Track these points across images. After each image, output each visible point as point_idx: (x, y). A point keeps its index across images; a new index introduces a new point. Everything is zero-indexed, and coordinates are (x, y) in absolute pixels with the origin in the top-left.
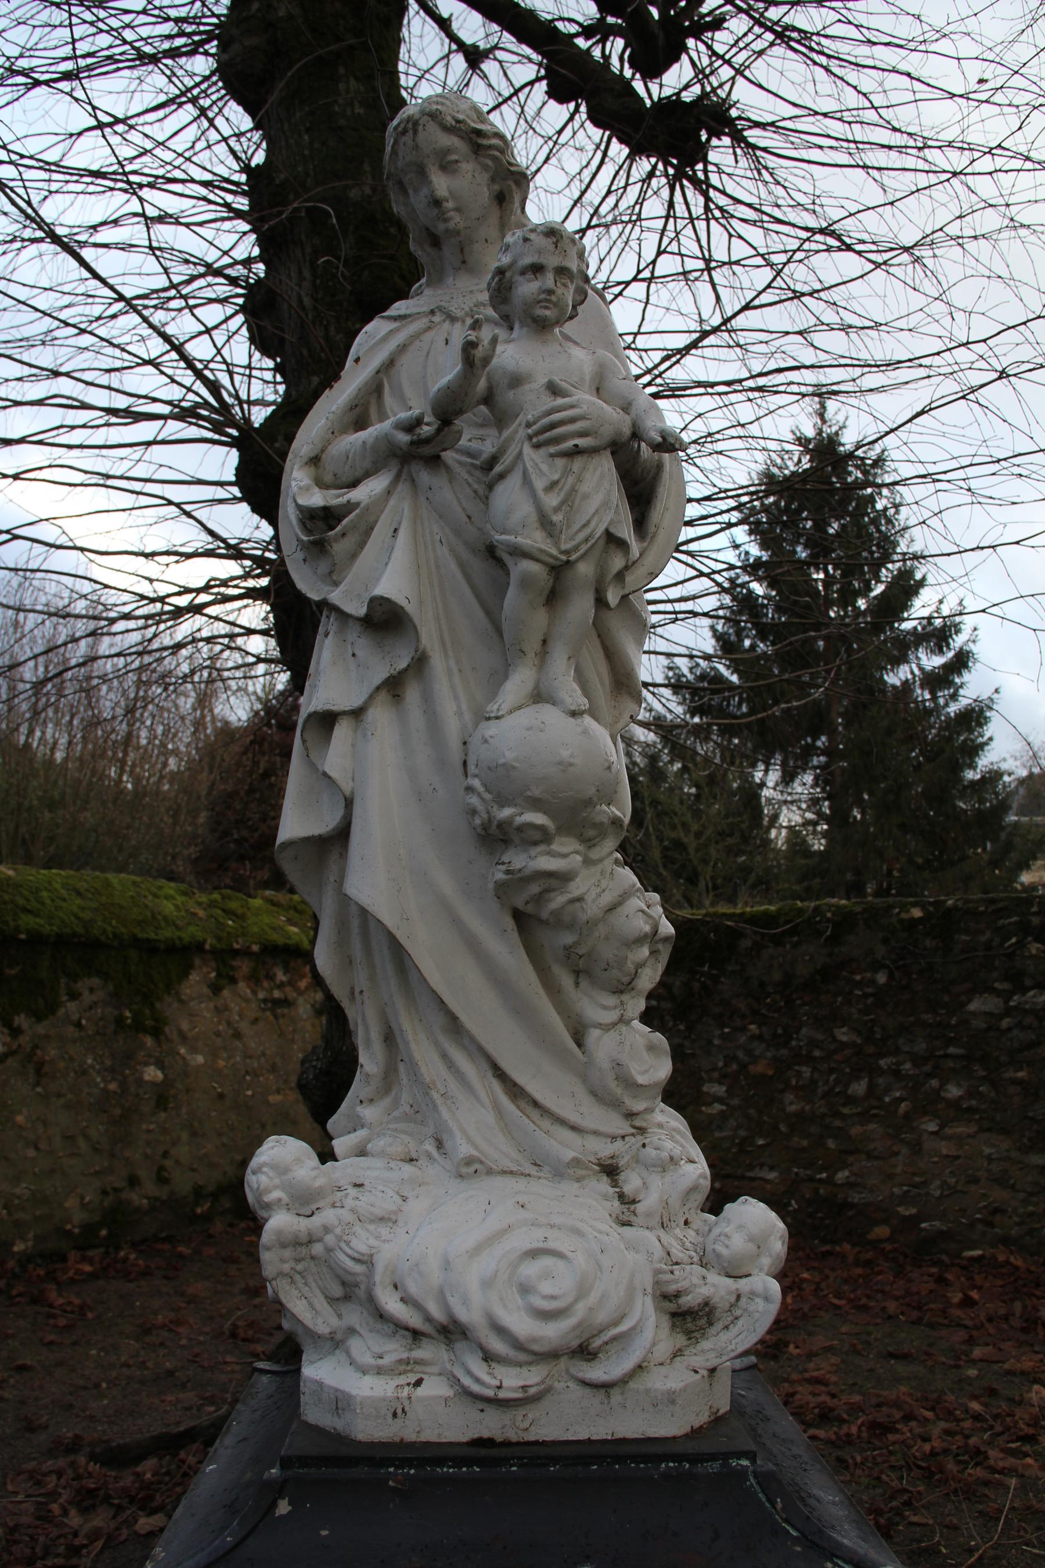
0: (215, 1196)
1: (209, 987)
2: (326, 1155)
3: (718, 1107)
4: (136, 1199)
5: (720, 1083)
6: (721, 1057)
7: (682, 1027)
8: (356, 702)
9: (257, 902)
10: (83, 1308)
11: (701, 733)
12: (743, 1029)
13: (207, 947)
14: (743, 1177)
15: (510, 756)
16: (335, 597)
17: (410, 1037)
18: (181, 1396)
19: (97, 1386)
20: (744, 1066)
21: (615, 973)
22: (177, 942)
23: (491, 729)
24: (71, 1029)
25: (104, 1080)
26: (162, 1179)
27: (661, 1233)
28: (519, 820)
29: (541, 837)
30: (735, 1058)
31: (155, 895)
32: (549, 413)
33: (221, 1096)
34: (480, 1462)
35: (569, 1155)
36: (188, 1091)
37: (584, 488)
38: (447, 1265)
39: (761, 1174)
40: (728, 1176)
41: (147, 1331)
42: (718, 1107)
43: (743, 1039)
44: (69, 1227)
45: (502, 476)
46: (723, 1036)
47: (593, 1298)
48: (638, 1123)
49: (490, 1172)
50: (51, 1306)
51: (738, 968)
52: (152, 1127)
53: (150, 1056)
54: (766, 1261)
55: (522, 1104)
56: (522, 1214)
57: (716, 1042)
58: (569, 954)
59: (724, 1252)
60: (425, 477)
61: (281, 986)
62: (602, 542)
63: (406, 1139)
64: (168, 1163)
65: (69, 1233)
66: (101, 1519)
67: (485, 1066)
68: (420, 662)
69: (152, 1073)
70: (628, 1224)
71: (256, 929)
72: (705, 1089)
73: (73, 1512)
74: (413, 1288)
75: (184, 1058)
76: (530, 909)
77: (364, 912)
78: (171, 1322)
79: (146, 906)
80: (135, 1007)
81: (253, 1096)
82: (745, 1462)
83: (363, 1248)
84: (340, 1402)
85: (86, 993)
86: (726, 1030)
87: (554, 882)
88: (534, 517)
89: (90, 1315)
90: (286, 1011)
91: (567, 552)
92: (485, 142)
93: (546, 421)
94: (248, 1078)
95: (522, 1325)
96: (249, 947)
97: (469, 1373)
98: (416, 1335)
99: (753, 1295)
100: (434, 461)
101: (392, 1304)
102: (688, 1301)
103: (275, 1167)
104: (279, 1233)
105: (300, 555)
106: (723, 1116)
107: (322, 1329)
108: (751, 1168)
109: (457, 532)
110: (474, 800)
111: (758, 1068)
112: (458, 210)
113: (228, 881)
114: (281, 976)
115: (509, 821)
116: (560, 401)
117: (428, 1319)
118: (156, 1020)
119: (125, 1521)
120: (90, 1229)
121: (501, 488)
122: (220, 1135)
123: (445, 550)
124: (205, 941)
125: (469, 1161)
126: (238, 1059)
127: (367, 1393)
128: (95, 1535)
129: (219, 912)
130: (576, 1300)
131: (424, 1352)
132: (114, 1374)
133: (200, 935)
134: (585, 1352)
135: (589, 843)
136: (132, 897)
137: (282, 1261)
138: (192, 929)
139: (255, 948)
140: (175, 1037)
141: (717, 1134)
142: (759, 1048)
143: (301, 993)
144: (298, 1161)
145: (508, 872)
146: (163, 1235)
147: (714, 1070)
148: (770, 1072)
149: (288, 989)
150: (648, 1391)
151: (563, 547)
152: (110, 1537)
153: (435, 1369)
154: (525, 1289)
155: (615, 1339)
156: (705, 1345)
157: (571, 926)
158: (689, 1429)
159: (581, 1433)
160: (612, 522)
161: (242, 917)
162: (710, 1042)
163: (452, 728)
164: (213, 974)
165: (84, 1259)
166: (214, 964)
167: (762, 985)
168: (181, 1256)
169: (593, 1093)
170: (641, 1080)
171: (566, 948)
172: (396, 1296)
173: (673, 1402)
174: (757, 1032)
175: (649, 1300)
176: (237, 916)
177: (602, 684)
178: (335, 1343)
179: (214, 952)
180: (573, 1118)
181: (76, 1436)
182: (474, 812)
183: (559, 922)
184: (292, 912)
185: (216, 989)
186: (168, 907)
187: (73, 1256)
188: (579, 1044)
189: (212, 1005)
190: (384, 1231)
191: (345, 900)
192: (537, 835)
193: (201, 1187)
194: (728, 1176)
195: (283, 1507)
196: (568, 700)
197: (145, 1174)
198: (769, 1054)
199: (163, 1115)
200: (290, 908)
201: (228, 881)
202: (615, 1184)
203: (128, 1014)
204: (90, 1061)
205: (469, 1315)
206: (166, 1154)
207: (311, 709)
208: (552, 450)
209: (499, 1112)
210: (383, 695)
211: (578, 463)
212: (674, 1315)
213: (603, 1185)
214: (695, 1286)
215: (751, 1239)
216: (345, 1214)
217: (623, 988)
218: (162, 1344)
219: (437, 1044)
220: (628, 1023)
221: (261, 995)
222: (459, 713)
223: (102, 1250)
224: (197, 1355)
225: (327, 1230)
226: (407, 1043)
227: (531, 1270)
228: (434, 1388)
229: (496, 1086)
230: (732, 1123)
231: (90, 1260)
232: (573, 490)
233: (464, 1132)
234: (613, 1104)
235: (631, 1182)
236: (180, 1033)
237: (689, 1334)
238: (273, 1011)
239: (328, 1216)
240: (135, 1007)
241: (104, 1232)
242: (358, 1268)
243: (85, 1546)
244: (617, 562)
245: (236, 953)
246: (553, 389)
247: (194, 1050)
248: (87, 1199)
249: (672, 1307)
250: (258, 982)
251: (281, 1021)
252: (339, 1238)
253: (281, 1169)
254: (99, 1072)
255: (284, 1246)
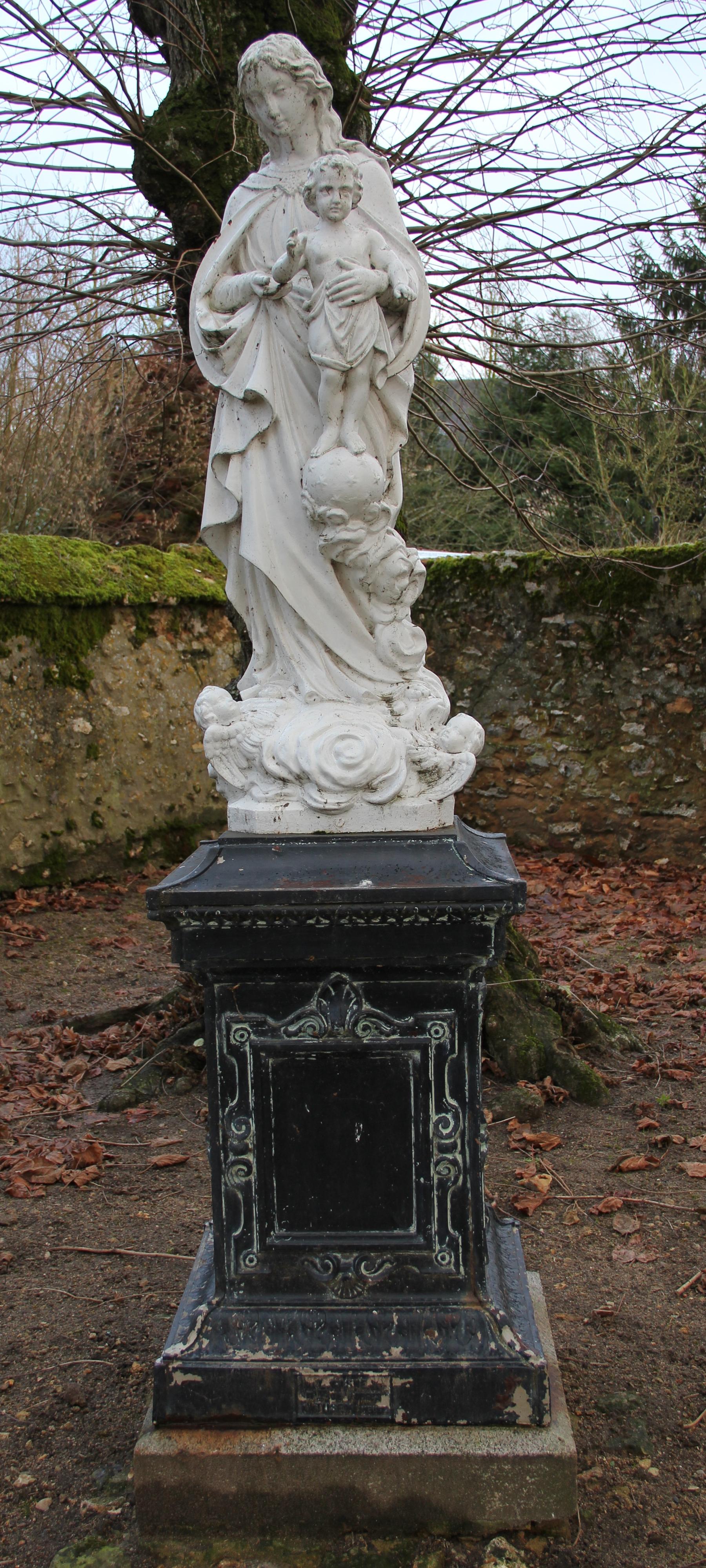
0: (147, 840)
1: (129, 640)
2: (237, 698)
3: (636, 746)
4: (74, 842)
5: (638, 723)
6: (639, 696)
7: (601, 667)
8: (241, 448)
9: (171, 556)
10: (37, 933)
11: (670, 331)
12: (661, 668)
13: (126, 602)
14: (661, 815)
15: (322, 479)
16: (225, 386)
17: (279, 631)
18: (131, 990)
19: (60, 984)
20: (662, 705)
21: (388, 593)
22: (97, 598)
23: (313, 464)
24: (4, 685)
25: (38, 733)
26: (97, 825)
27: (414, 732)
28: (329, 513)
29: (343, 521)
30: (653, 697)
31: (72, 553)
32: (338, 282)
33: (147, 745)
34: (317, 840)
35: (364, 690)
36: (116, 741)
37: (359, 324)
38: (299, 744)
39: (679, 812)
40: (647, 814)
41: (98, 947)
42: (636, 746)
43: (661, 678)
44: (15, 868)
45: (314, 318)
46: (641, 676)
47: (373, 759)
48: (407, 677)
49: (322, 700)
50: (8, 930)
51: (656, 606)
52: (84, 775)
53: (78, 708)
54: (469, 745)
55: (342, 667)
57: (634, 681)
58: (362, 583)
59: (446, 740)
60: (273, 310)
61: (199, 638)
62: (371, 354)
63: (279, 687)
64: (101, 809)
65: (15, 874)
66: (79, 1061)
67: (320, 646)
68: (275, 424)
69: (82, 725)
70: (396, 726)
71: (172, 582)
72: (623, 728)
73: (57, 1058)
74: (282, 757)
75: (110, 710)
76: (339, 559)
77: (251, 565)
78: (116, 940)
79: (65, 565)
80: (62, 662)
81: (177, 745)
82: (451, 840)
83: (256, 740)
84: (247, 817)
85: (15, 651)
86: (645, 669)
87: (350, 545)
88: (331, 344)
89: (43, 937)
90: (206, 662)
91: (351, 362)
93: (336, 287)
94: (172, 728)
95: (336, 772)
96: (166, 601)
97: (311, 797)
98: (284, 781)
99: (461, 762)
100: (279, 301)
101: (272, 766)
102: (426, 765)
103: (209, 701)
104: (213, 734)
105: (204, 355)
106: (641, 754)
107: (238, 784)
108: (669, 805)
109: (293, 345)
110: (306, 503)
111: (677, 706)
113: (134, 533)
114: (199, 627)
115: (324, 513)
116: (345, 273)
117: (291, 772)
118: (82, 674)
119: (98, 1063)
120: (33, 870)
121: (314, 325)
122: (149, 782)
123: (286, 355)
124: (123, 596)
125: (311, 695)
126: (162, 709)
127: (261, 810)
128: (76, 1071)
129: (135, 567)
130: (364, 760)
131: (290, 789)
132: (72, 976)
133: (118, 591)
134: (370, 788)
135: (370, 523)
136: (51, 556)
137: (216, 749)
138: (110, 585)
139: (173, 601)
140: (100, 689)
141: (635, 773)
142: (677, 687)
143: (219, 644)
144: (221, 697)
145: (325, 540)
146: (101, 876)
147: (632, 709)
148: (688, 711)
149: (206, 640)
151: (349, 359)
152: (88, 1073)
153: (295, 799)
154: (338, 754)
155: (384, 780)
156: (437, 788)
157: (362, 568)
159: (370, 829)
160: (376, 341)
161: (158, 571)
162: (629, 682)
163: (294, 461)
164: (134, 628)
165: (30, 896)
166: (133, 618)
167: (680, 622)
168: (119, 893)
169: (381, 660)
170: (406, 652)
171: (361, 580)
172: (274, 762)
173: (416, 813)
174: (675, 670)
175: (403, 763)
176: (152, 570)
177: (381, 428)
178: (243, 792)
179: (132, 606)
180: (369, 673)
181: (51, 1012)
182: (306, 509)
183: (355, 566)
184: (206, 564)
185: (137, 643)
186: (86, 565)
187: (20, 894)
188: (372, 633)
189: (133, 658)
190: (268, 732)
191: (241, 559)
192: (339, 521)
193: (133, 831)
194: (647, 814)
195: (221, 860)
196: (353, 446)
197: (81, 819)
198: (687, 693)
199: (94, 764)
200: (204, 559)
201: (134, 533)
202: (390, 706)
203: (55, 669)
204: (23, 715)
205: (310, 767)
206: (98, 801)
207: (216, 452)
208: (340, 303)
209: (328, 670)
210: (256, 443)
211: (355, 310)
212: (420, 772)
213: (384, 706)
215: (461, 733)
216: (247, 724)
217: (396, 601)
218: (110, 957)
219: (294, 635)
220: (400, 621)
221: (181, 647)
222: (298, 453)
223: (46, 889)
224: (142, 962)
225: (238, 732)
226: (277, 635)
227: (340, 745)
228: (295, 807)
229: (327, 657)
230: (650, 761)
231: (37, 898)
232: (353, 326)
233: (309, 681)
234: (393, 666)
235: (398, 706)
236: (106, 685)
237: (429, 783)
238: (192, 662)
239: (238, 725)
240: (62, 662)
241: (47, 873)
242: (254, 750)
243: (70, 1077)
244: (381, 364)
245: (154, 606)
246: (341, 266)
247: (119, 702)
248: (30, 842)
249: (418, 768)
250: (176, 633)
251: (201, 672)
252: (244, 736)
253: (213, 702)
254: (32, 725)
255: (216, 741)
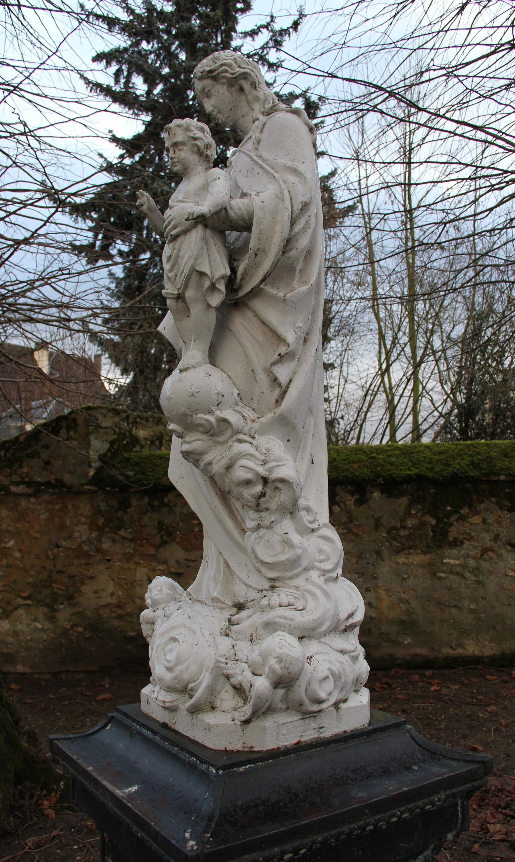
56: (187, 622)
92: (215, 74)
112: (219, 112)
130: (176, 665)
150: (203, 720)
158: (224, 749)
214: (236, 674)
